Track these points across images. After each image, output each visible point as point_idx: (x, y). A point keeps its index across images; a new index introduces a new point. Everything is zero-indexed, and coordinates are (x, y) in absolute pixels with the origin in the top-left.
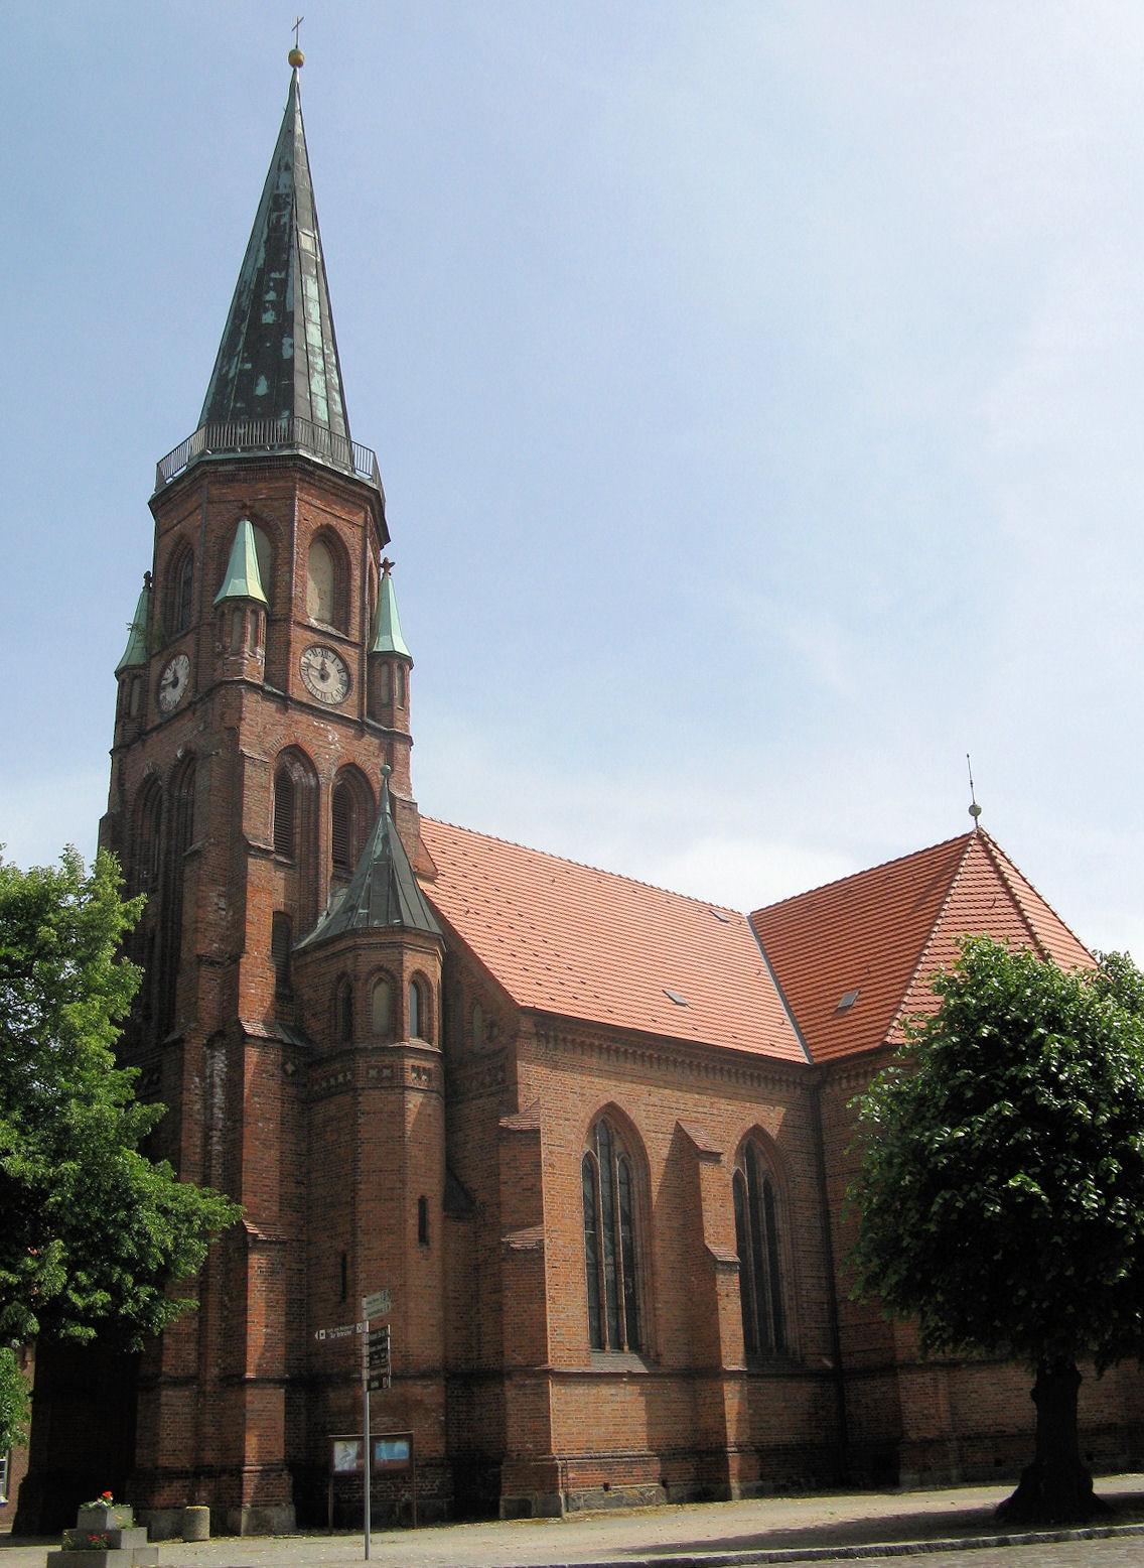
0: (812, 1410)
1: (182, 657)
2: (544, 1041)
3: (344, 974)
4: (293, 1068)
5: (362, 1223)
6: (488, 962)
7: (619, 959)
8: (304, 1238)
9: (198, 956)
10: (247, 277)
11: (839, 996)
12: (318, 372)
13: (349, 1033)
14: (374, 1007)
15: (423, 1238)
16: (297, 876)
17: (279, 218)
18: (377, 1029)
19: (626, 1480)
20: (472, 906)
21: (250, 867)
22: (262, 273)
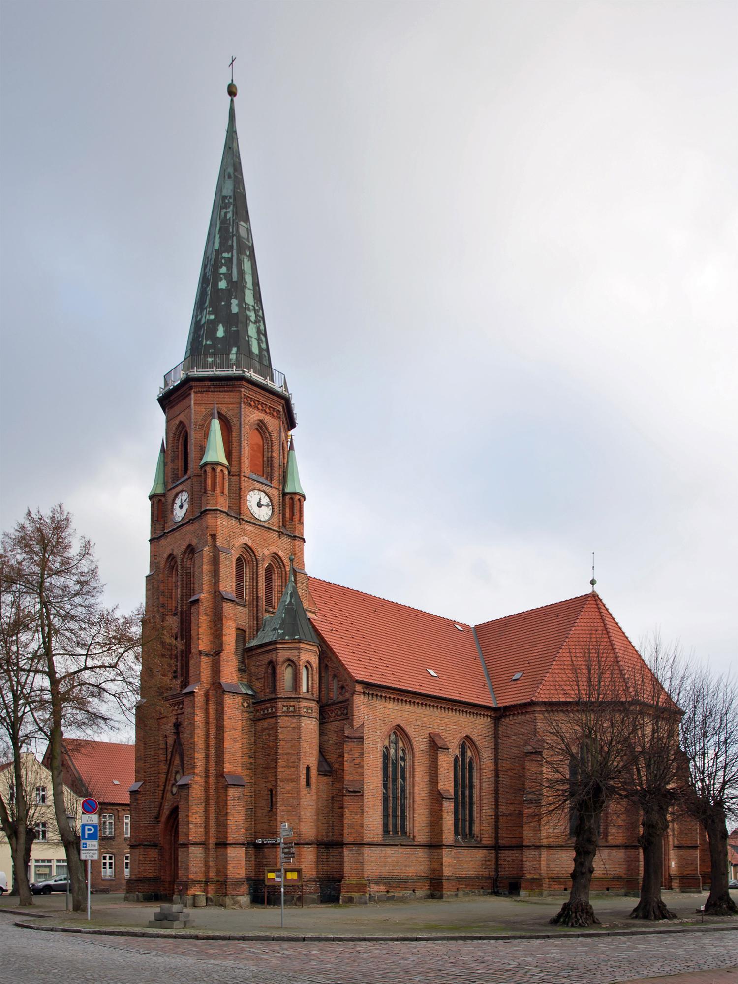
0: (484, 862)
1: (184, 492)
2: (367, 696)
4: (247, 704)
5: (279, 777)
6: (341, 656)
7: (411, 671)
8: (253, 781)
12: (252, 322)
13: (274, 690)
15: (308, 784)
16: (247, 610)
17: (226, 213)
20: (334, 626)
21: (225, 609)
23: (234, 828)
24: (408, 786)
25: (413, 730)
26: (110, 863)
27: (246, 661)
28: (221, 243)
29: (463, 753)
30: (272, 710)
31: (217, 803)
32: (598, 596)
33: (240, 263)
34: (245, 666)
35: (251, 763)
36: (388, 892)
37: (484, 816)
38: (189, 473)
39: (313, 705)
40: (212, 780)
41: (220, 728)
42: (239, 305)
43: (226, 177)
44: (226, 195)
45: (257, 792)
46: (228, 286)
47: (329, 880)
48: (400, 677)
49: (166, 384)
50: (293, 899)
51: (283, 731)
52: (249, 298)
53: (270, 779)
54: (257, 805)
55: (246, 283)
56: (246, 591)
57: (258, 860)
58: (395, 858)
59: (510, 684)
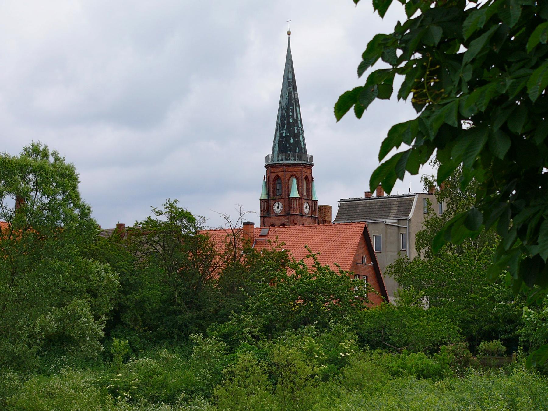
17: (290, 89)
33: (296, 110)
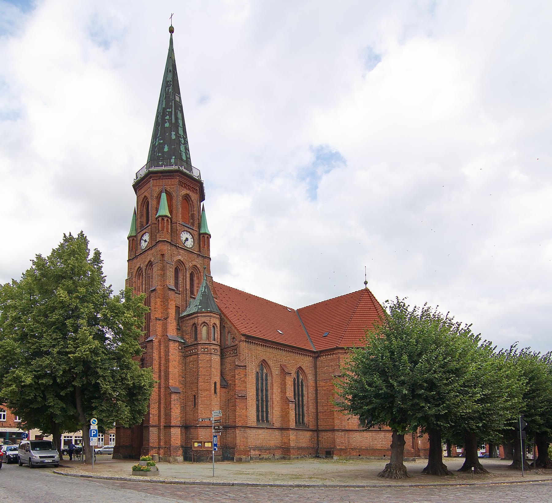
1: (147, 233)
3: (194, 324)
5: (200, 388)
9: (156, 318)
10: (160, 110)
11: (323, 333)
13: (196, 339)
14: (203, 332)
15: (215, 392)
17: (168, 90)
18: (203, 338)
19: (265, 454)
22: (164, 110)
23: (174, 417)
24: (269, 394)
25: (272, 363)
26: (102, 438)
27: (180, 324)
28: (166, 104)
29: (298, 377)
30: (195, 350)
31: (166, 402)
32: (369, 290)
34: (180, 327)
35: (183, 381)
36: (260, 455)
37: (310, 413)
38: (150, 222)
39: (218, 348)
40: (162, 390)
41: (167, 361)
42: (176, 135)
43: (169, 72)
44: (169, 80)
45: (187, 397)
46: (170, 126)
47: (227, 448)
48: (264, 333)
49: (137, 177)
50: (208, 459)
51: (201, 362)
52: (181, 132)
53: (194, 389)
54: (186, 404)
55: (179, 124)
56: (180, 286)
57: (187, 436)
58: (263, 436)
59: (322, 338)
